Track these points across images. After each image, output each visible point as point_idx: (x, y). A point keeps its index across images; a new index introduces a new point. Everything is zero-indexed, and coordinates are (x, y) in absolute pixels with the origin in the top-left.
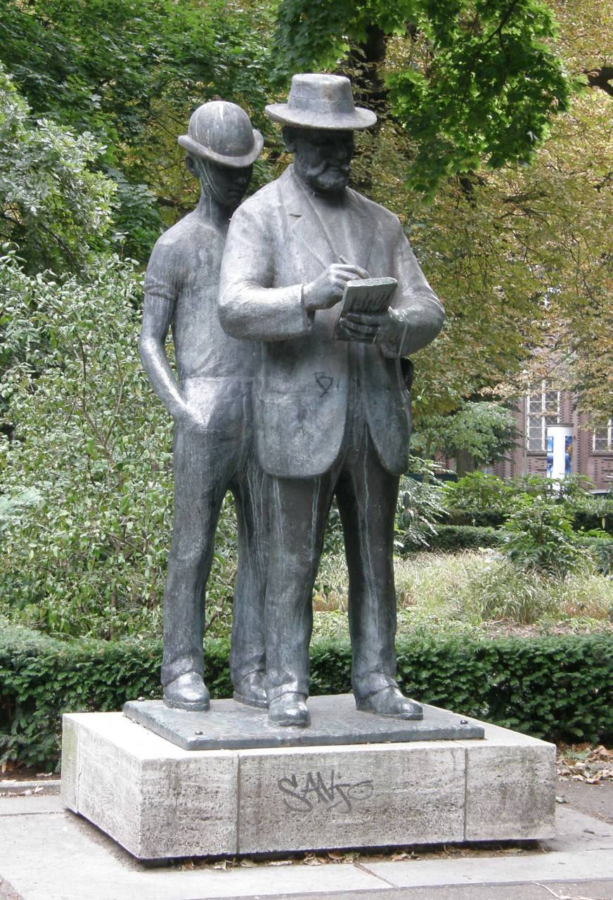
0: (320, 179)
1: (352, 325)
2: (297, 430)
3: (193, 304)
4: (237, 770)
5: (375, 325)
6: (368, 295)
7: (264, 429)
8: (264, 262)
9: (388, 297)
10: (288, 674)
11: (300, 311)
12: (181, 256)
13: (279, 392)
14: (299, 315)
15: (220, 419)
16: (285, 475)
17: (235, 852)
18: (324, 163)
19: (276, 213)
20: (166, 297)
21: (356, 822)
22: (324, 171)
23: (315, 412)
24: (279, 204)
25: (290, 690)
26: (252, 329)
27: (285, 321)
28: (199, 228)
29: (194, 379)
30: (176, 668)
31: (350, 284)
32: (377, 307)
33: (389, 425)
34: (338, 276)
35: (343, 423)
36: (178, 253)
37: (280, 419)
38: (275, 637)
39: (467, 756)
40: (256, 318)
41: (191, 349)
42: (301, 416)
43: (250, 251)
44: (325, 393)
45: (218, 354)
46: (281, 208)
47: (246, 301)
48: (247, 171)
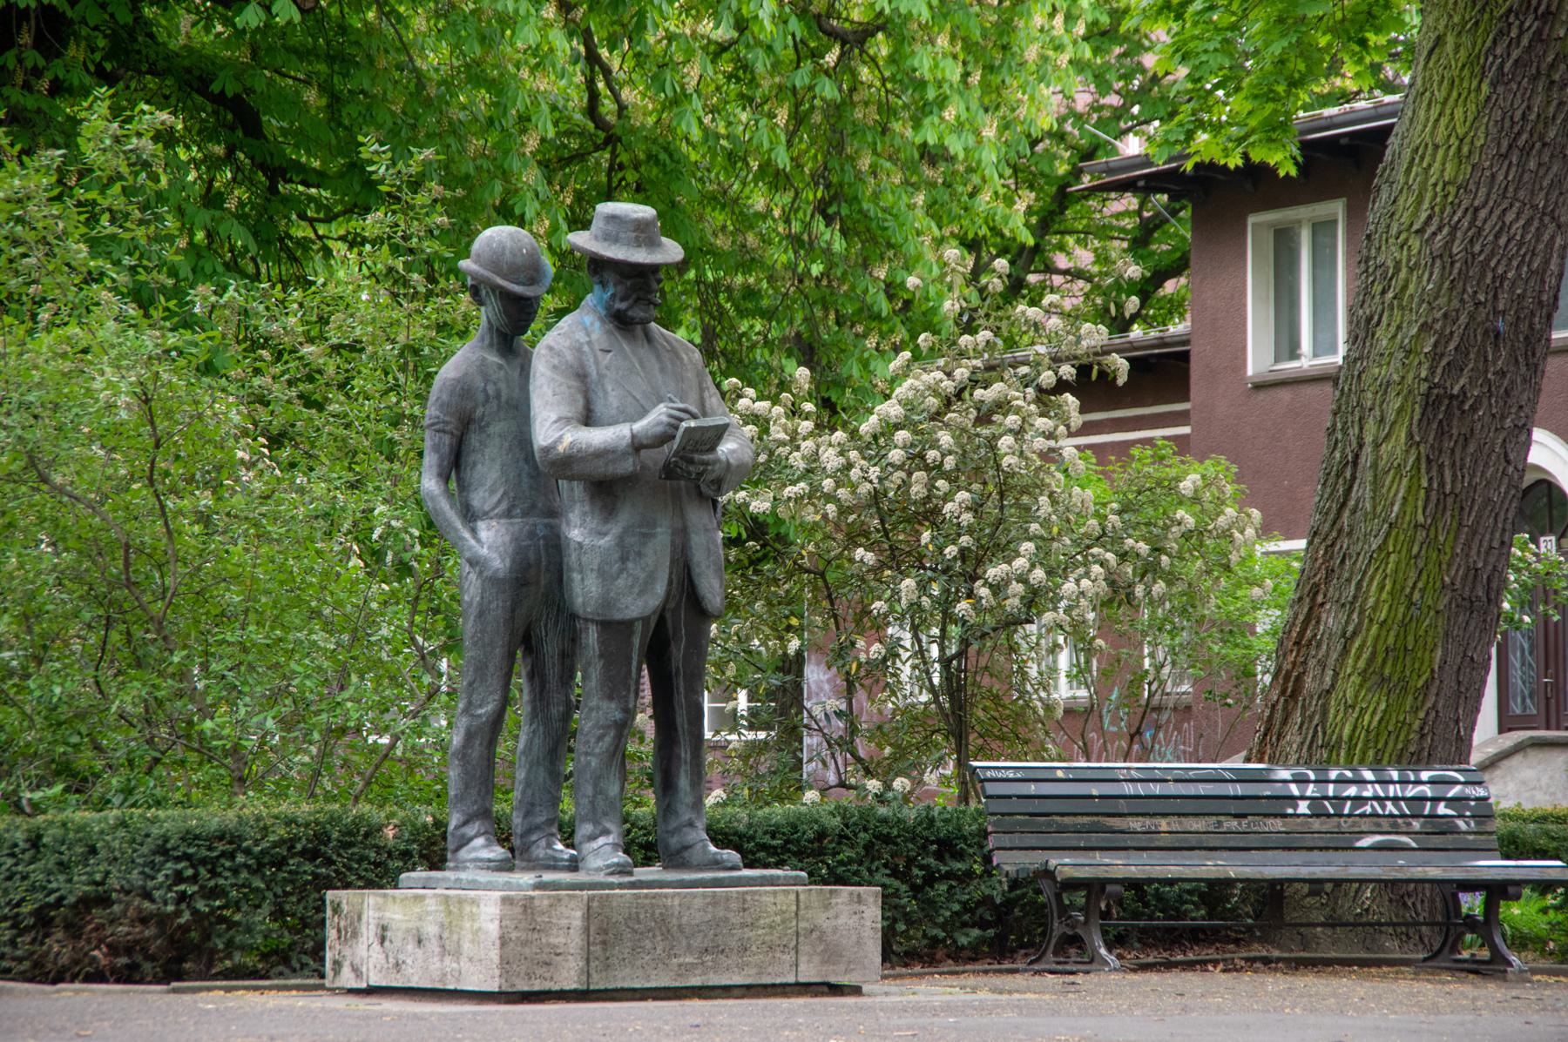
2: (621, 571)
5: (707, 463)
8: (581, 402)
19: (586, 348)
23: (639, 554)
34: (671, 416)
42: (624, 559)
43: (563, 388)
44: (646, 537)
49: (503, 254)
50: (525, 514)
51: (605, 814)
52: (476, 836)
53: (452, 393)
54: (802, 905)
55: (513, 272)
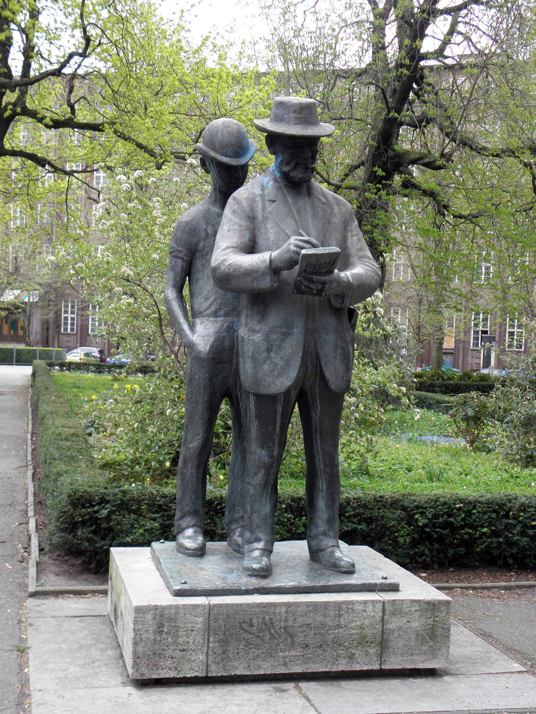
0: (291, 174)
1: (306, 283)
3: (202, 265)
4: (207, 615)
5: (324, 283)
6: (318, 260)
7: (243, 358)
9: (333, 263)
11: (268, 271)
12: (195, 230)
13: (254, 331)
14: (267, 274)
15: (217, 348)
16: (257, 392)
17: (204, 675)
18: (294, 162)
20: (183, 259)
21: (298, 654)
22: (295, 168)
23: (279, 347)
24: (261, 192)
25: (258, 547)
26: (234, 284)
27: (257, 279)
28: (209, 209)
30: (184, 523)
31: (303, 252)
32: (325, 270)
33: (335, 358)
34: (297, 246)
35: (301, 355)
37: (254, 351)
38: (249, 508)
39: (384, 605)
40: (236, 275)
41: (200, 297)
42: (269, 350)
43: (236, 227)
44: (285, 335)
45: (219, 301)
46: (262, 196)
47: (230, 262)
49: (216, 135)
50: (227, 315)
51: (258, 527)
52: (187, 527)
53: (183, 232)
54: (387, 612)
55: (222, 149)
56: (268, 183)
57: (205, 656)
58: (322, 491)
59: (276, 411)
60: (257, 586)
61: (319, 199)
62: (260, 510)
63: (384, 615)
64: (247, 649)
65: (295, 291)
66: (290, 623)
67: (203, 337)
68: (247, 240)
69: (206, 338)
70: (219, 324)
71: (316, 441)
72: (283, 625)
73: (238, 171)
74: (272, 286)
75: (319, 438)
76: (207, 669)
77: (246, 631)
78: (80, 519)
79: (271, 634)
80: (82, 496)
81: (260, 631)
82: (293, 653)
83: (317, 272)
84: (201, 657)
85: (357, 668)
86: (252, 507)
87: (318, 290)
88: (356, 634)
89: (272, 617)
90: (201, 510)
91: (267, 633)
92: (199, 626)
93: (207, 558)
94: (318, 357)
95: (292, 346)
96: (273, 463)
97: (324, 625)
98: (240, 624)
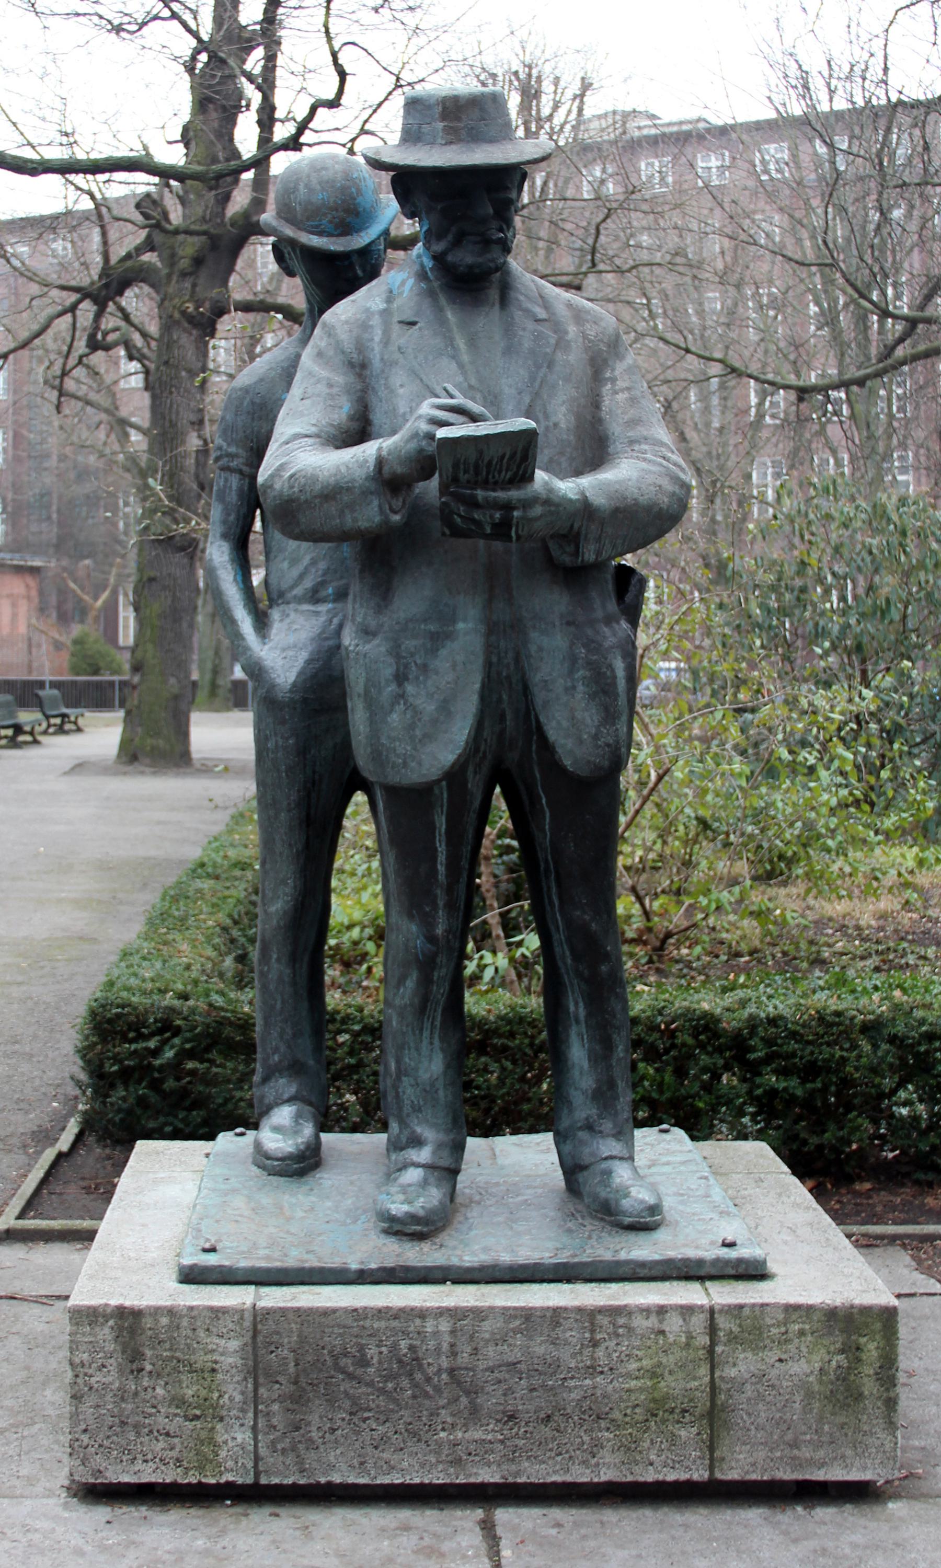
1: (462, 509)
4: (250, 1334)
5: (508, 507)
6: (481, 453)
10: (414, 1132)
11: (373, 486)
17: (250, 1480)
18: (454, 229)
20: (241, 472)
21: (489, 1437)
22: (457, 242)
24: (382, 306)
27: (351, 506)
29: (282, 607)
30: (269, 1092)
31: (441, 433)
35: (477, 686)
36: (258, 401)
37: (368, 680)
40: (306, 501)
42: (400, 678)
43: (322, 388)
44: (437, 640)
45: (322, 565)
48: (365, 252)
51: (417, 1109)
56: (403, 283)
57: (249, 1434)
58: (577, 1022)
59: (432, 827)
60: (390, 1263)
61: (527, 311)
62: (416, 1069)
63: (713, 1343)
64: (355, 1419)
65: (447, 532)
66: (464, 1358)
67: (284, 650)
68: (344, 417)
69: (291, 653)
70: (323, 619)
71: (550, 898)
72: (445, 1363)
73: (351, 266)
74: (386, 522)
75: (554, 890)
76: (256, 1466)
77: (351, 1376)
78: (115, 1068)
79: (415, 1385)
80: (118, 1016)
81: (386, 1379)
82: (478, 1434)
83: (486, 482)
84: (240, 1437)
85: (650, 1476)
86: (398, 1062)
87: (495, 526)
88: (641, 1390)
89: (418, 1343)
90: (311, 1062)
91: (405, 1383)
92: (230, 1360)
93: (326, 1178)
94: (526, 689)
95: (454, 666)
96: (435, 955)
97: (555, 1366)
98: (335, 1358)
